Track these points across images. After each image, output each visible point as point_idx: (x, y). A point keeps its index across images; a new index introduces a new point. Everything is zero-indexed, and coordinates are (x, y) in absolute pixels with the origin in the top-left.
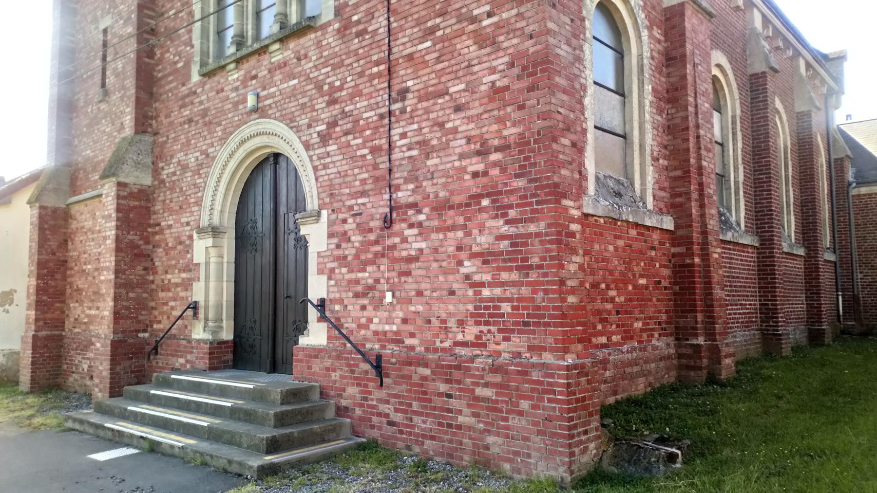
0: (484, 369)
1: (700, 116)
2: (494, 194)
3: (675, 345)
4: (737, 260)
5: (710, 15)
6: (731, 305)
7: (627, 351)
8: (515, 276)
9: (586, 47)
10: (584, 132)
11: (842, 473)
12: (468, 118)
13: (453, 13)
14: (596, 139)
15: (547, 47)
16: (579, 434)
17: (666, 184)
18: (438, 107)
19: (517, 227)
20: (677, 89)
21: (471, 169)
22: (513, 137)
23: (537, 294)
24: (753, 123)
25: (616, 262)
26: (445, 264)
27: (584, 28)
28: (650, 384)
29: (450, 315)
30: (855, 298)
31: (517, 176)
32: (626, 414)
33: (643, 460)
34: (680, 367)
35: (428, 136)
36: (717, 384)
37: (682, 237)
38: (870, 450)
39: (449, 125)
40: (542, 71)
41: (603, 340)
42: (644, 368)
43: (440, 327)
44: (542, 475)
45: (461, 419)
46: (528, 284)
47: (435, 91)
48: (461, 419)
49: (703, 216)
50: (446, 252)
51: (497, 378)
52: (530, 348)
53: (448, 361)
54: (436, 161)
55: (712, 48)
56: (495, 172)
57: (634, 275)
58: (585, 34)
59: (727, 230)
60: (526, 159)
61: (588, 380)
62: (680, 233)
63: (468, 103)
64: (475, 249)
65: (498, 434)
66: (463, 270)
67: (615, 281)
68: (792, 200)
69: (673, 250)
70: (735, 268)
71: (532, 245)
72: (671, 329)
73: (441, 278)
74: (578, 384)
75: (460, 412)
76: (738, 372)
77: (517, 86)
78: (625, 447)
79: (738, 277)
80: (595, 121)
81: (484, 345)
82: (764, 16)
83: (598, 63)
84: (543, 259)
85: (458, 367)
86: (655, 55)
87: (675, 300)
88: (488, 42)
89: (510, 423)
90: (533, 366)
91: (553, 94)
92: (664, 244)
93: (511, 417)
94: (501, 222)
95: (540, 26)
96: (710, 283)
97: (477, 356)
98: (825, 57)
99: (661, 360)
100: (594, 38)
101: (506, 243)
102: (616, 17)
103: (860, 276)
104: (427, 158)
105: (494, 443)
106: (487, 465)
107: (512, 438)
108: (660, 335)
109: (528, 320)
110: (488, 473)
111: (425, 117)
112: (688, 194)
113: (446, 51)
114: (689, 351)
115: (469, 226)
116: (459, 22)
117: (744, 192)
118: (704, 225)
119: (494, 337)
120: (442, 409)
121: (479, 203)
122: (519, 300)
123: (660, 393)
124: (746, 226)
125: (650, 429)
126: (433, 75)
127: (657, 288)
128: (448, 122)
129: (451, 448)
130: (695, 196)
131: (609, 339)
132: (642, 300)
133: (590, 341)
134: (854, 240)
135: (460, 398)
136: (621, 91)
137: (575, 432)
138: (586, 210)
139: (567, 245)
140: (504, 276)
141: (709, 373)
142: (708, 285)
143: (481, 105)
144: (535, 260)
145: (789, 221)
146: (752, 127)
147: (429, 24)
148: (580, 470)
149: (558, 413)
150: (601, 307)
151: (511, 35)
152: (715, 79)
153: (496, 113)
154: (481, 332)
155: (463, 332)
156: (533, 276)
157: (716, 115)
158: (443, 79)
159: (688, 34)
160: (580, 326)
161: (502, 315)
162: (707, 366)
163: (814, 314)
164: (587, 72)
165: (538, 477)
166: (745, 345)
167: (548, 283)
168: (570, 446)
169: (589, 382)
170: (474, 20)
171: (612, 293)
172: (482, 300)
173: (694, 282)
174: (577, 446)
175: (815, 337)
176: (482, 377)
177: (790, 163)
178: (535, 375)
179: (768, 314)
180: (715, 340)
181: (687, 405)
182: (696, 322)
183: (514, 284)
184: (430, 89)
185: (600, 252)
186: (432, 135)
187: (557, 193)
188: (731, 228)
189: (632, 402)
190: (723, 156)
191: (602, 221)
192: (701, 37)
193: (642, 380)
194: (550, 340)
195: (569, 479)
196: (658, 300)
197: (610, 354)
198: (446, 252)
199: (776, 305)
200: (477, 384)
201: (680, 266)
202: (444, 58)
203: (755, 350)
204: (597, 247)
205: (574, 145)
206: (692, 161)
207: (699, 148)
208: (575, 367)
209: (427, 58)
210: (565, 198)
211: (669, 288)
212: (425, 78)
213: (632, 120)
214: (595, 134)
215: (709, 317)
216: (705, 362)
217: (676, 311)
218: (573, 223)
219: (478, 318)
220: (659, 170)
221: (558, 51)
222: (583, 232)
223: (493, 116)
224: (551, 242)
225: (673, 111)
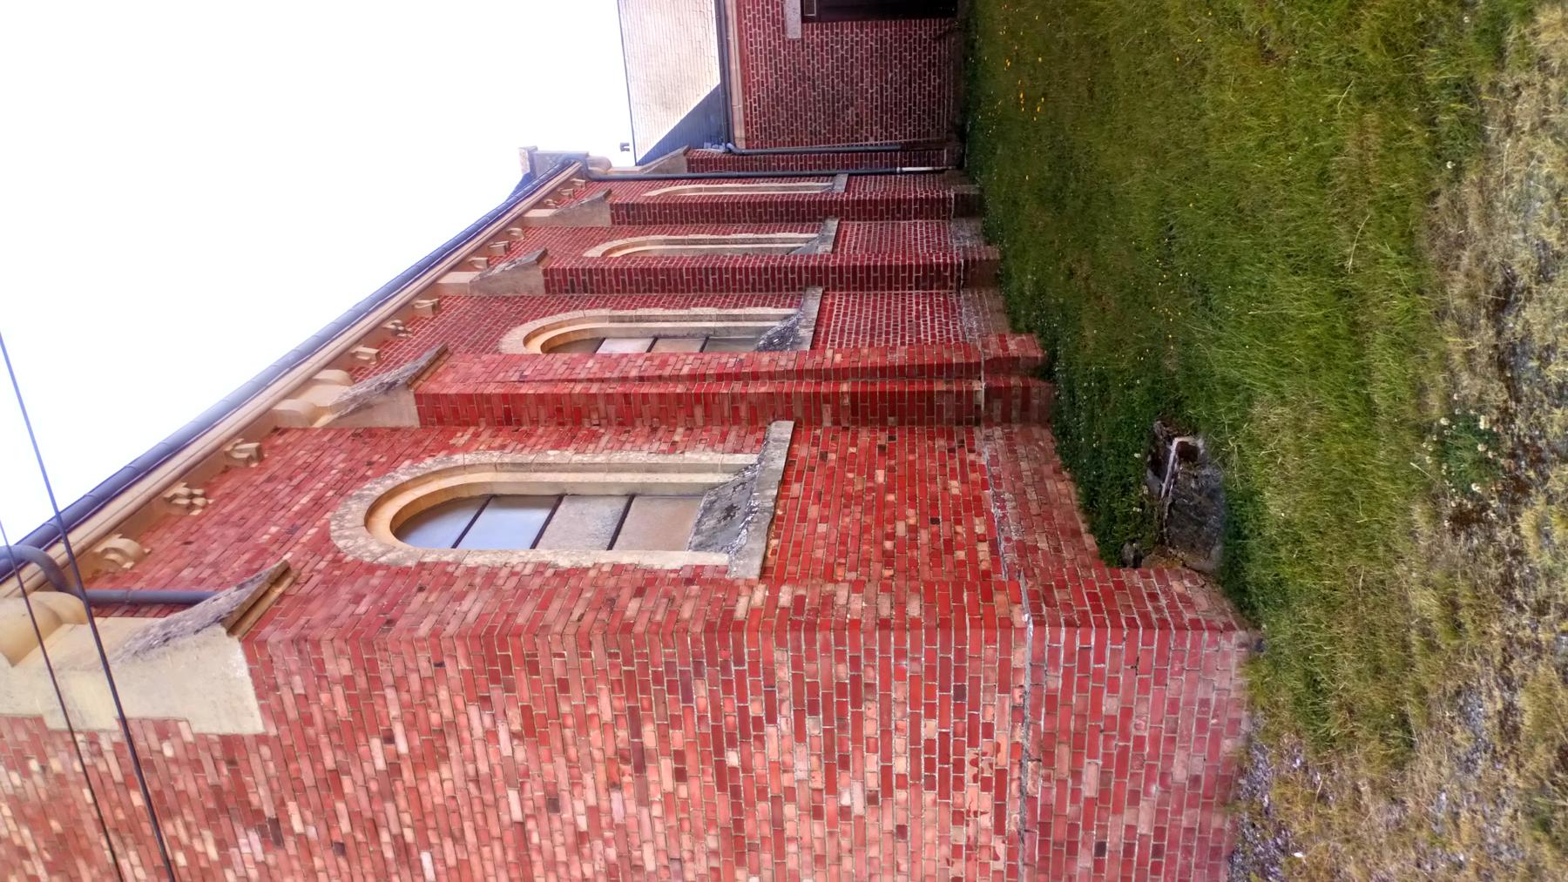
0: (1047, 778)
1: (608, 375)
2: (718, 741)
3: (988, 427)
4: (844, 322)
5: (443, 353)
6: (919, 333)
7: (1002, 508)
8: (871, 710)
9: (470, 562)
10: (618, 569)
11: (1197, 200)
12: (573, 785)
13: (376, 808)
14: (630, 546)
15: (460, 636)
16: (1158, 610)
17: (716, 431)
18: (546, 844)
19: (782, 701)
20: (560, 410)
21: (668, 784)
22: (616, 703)
23: (904, 672)
24: (624, 291)
25: (847, 520)
26: (845, 843)
27: (436, 564)
28: (1057, 472)
29: (943, 839)
30: (905, 148)
31: (688, 698)
32: (1114, 520)
33: (1195, 502)
34: (1025, 420)
35: (600, 865)
36: (1051, 366)
37: (806, 409)
38: (1156, 155)
39: (583, 823)
40: (503, 646)
41: (983, 548)
42: (1030, 481)
43: (968, 859)
44: (1240, 681)
45: (1144, 828)
46: (886, 685)
47: (516, 850)
48: (1144, 828)
49: (771, 376)
50: (823, 840)
51: (1063, 753)
52: (1005, 688)
53: (1031, 846)
54: (648, 851)
55: (497, 351)
56: (677, 738)
57: (870, 490)
58: (448, 564)
59: (796, 336)
60: (658, 679)
61: (1058, 587)
62: (798, 412)
63: (545, 786)
64: (819, 783)
65: (1169, 758)
66: (859, 807)
67: (880, 523)
68: (751, 236)
69: (827, 423)
70: (858, 326)
71: (815, 675)
72: (960, 432)
73: (873, 852)
74: (1067, 606)
75: (1131, 829)
76: (1030, 331)
77: (524, 692)
78: (1174, 530)
79: (873, 322)
80: (600, 547)
81: (1001, 774)
82: (453, 268)
83: (501, 540)
84: (840, 657)
85: (1045, 828)
86: (498, 441)
87: (912, 423)
88: (437, 744)
89: (1146, 734)
90: (1036, 684)
91: (546, 627)
92: (816, 438)
93: (1133, 732)
94: (770, 730)
95: (423, 649)
96: (883, 369)
97: (1021, 789)
98: (527, 178)
99: (1014, 452)
100: (455, 546)
101: (809, 722)
102: (425, 505)
103: (872, 141)
104: (640, 868)
105: (1186, 767)
106: (1227, 782)
107: (1175, 732)
108: (971, 451)
109: (952, 689)
110: (1242, 781)
111: (562, 870)
112: (734, 397)
113: (442, 824)
114: (997, 405)
115: (776, 792)
116: (393, 796)
117: (735, 306)
118: (787, 374)
119: (984, 754)
120: (1127, 864)
121: (734, 770)
122: (915, 703)
123: (1070, 458)
124: (790, 306)
125: (1138, 482)
126: (486, 850)
127: (892, 451)
128: (575, 824)
129: (1201, 852)
130: (737, 387)
131: (982, 539)
132: (912, 478)
133: (987, 574)
134: (815, 148)
135: (1103, 828)
136: (554, 501)
137: (1154, 616)
138: (754, 573)
139: (816, 612)
140: (871, 729)
141: (1033, 376)
142: (885, 371)
143: (551, 760)
144: (843, 672)
145: (784, 241)
146: (631, 291)
147: (389, 854)
148: (1223, 612)
149: (1123, 646)
150: (926, 550)
151: (432, 700)
152: (549, 348)
153: (568, 733)
154: (975, 778)
155: (975, 813)
156: (872, 676)
157: (606, 348)
158: (496, 831)
159: (470, 390)
160: (964, 596)
161: (944, 737)
162: (1022, 377)
163: (930, 209)
164: (514, 560)
165: (1241, 688)
166: (985, 314)
167: (884, 650)
168: (1181, 628)
169: (1062, 585)
170: (394, 769)
171: (901, 529)
172: (916, 775)
173: (882, 393)
174: (1180, 614)
175: (968, 208)
176: (1062, 783)
177: (691, 236)
178: (1055, 682)
179: (932, 277)
180: (978, 364)
181: (1092, 417)
182: (949, 392)
183: (885, 713)
184: (511, 857)
185: (829, 548)
186: (598, 857)
187: (723, 626)
188: (792, 329)
189: (1090, 503)
190: (675, 337)
191: (774, 542)
192: (477, 369)
193: (1050, 485)
194: (990, 652)
195: (1241, 633)
196: (912, 451)
197: (1008, 540)
198: (823, 840)
199: (918, 266)
200: (1076, 793)
201: (855, 412)
202: (455, 828)
203: (992, 300)
204: (820, 553)
205: (639, 592)
206: (680, 389)
207: (660, 377)
208: (1035, 610)
209: (451, 861)
210: (732, 612)
211: (892, 432)
212: (489, 868)
213: (605, 485)
214: (621, 549)
215: (940, 372)
216: (1014, 381)
217: (931, 423)
218: (776, 599)
219: (949, 784)
220: (692, 440)
221: (471, 617)
222: (792, 580)
223: (574, 737)
224: (811, 642)
225: (595, 416)
